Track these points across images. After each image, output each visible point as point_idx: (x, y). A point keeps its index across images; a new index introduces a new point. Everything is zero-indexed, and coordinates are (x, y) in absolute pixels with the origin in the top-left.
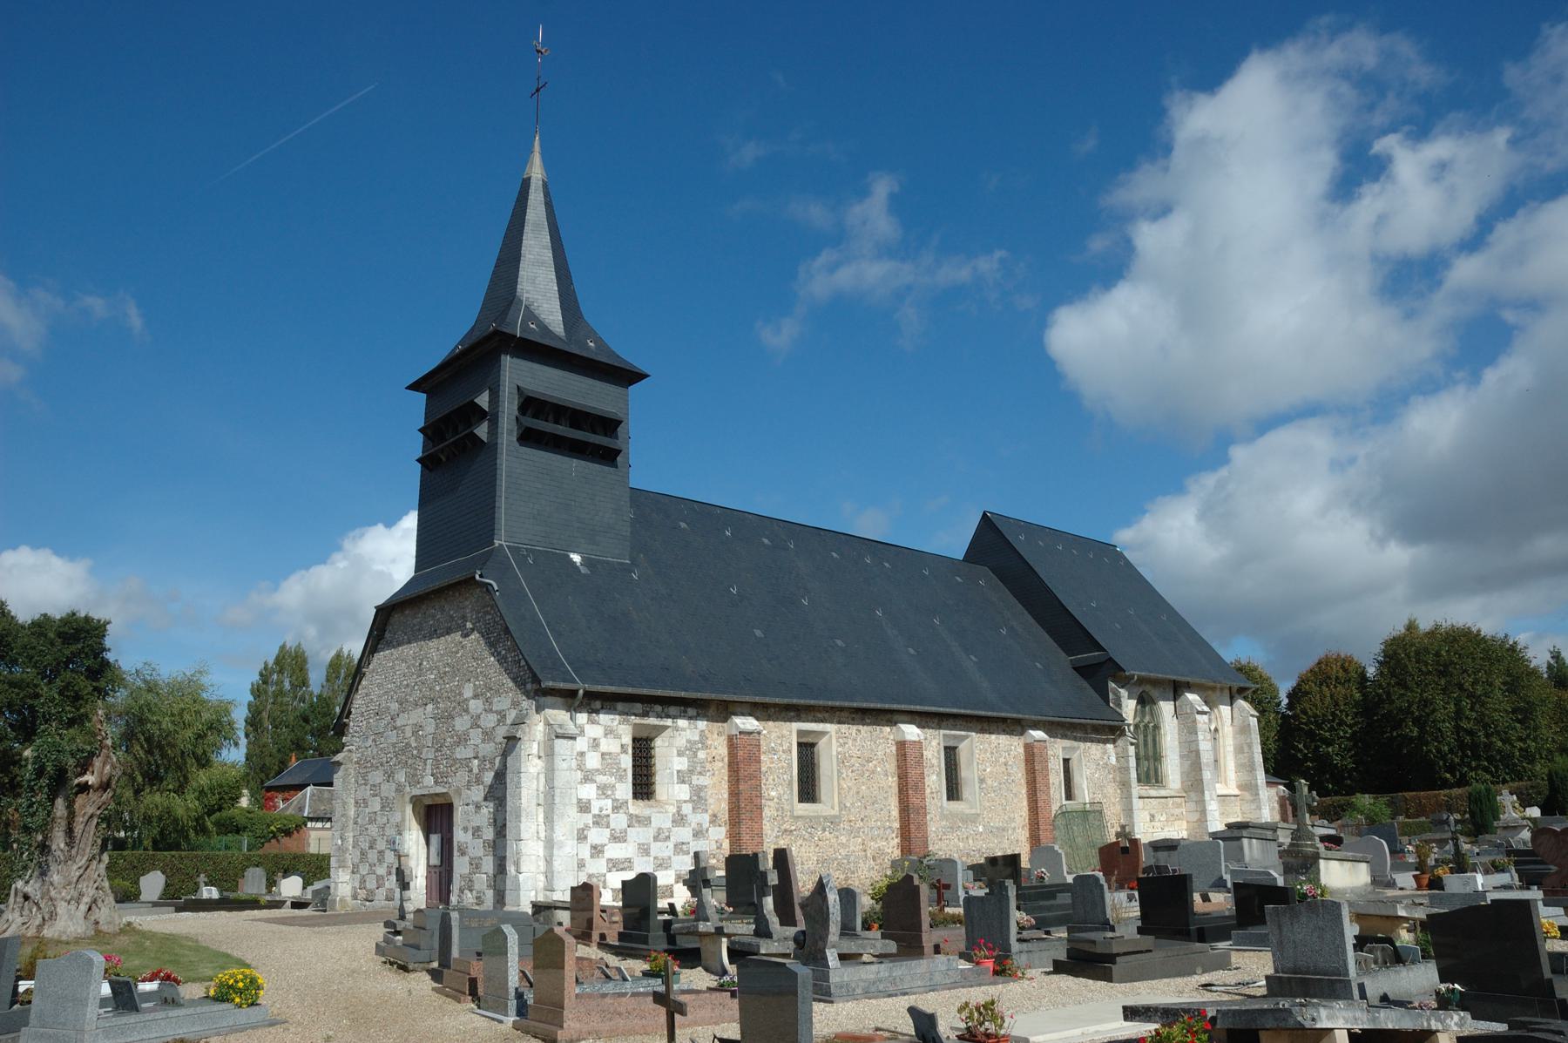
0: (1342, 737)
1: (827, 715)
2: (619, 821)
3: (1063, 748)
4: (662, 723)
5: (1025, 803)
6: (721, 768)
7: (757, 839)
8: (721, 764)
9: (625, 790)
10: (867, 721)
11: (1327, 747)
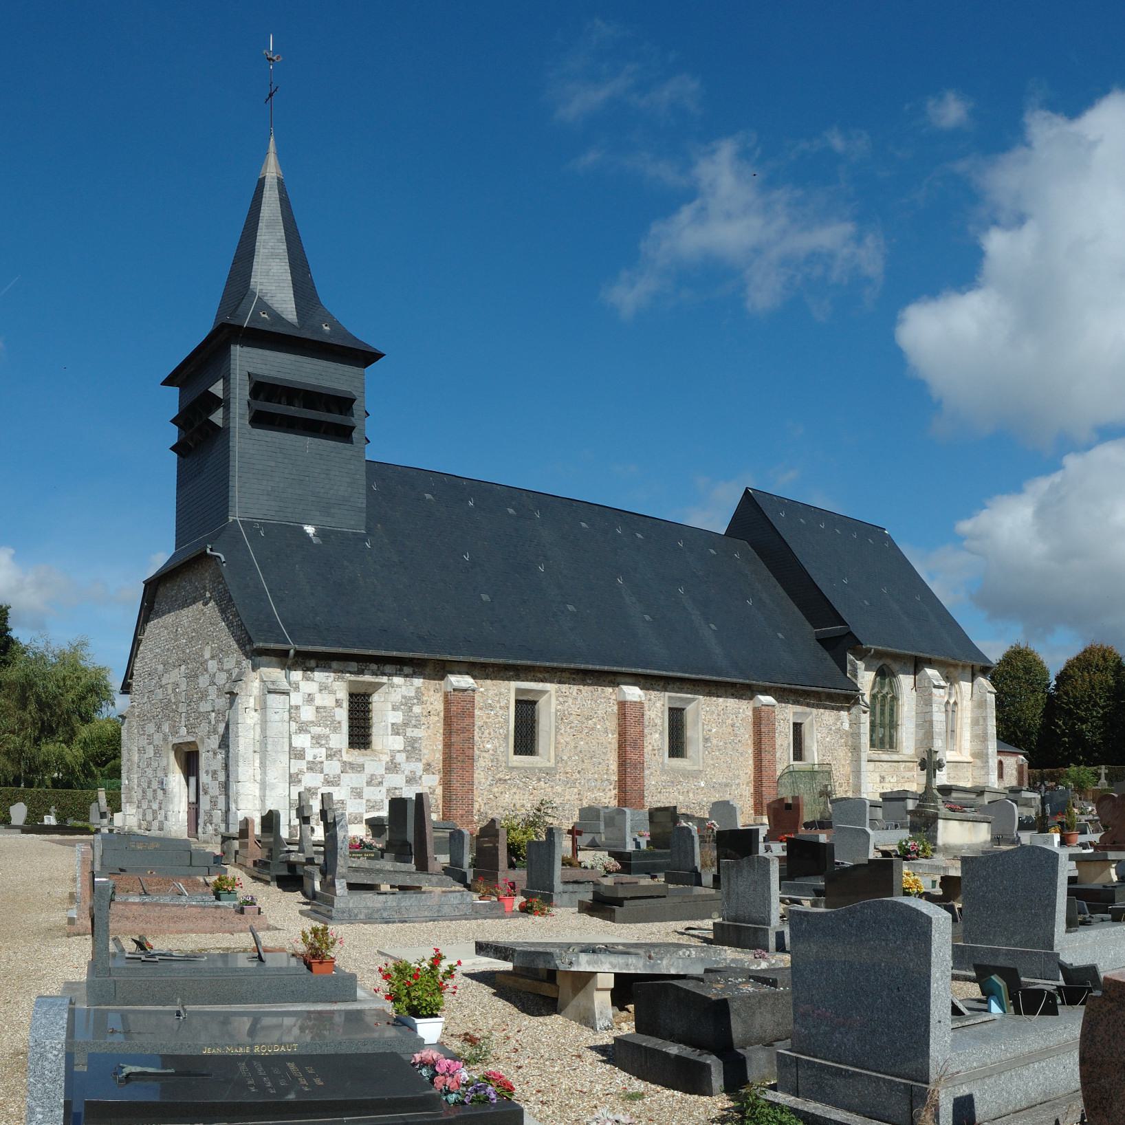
0: (1094, 717)
1: (547, 675)
2: (333, 767)
3: (793, 712)
4: (377, 680)
5: (751, 762)
6: (437, 722)
7: (467, 787)
8: (436, 718)
9: (340, 739)
10: (588, 681)
11: (1082, 725)
